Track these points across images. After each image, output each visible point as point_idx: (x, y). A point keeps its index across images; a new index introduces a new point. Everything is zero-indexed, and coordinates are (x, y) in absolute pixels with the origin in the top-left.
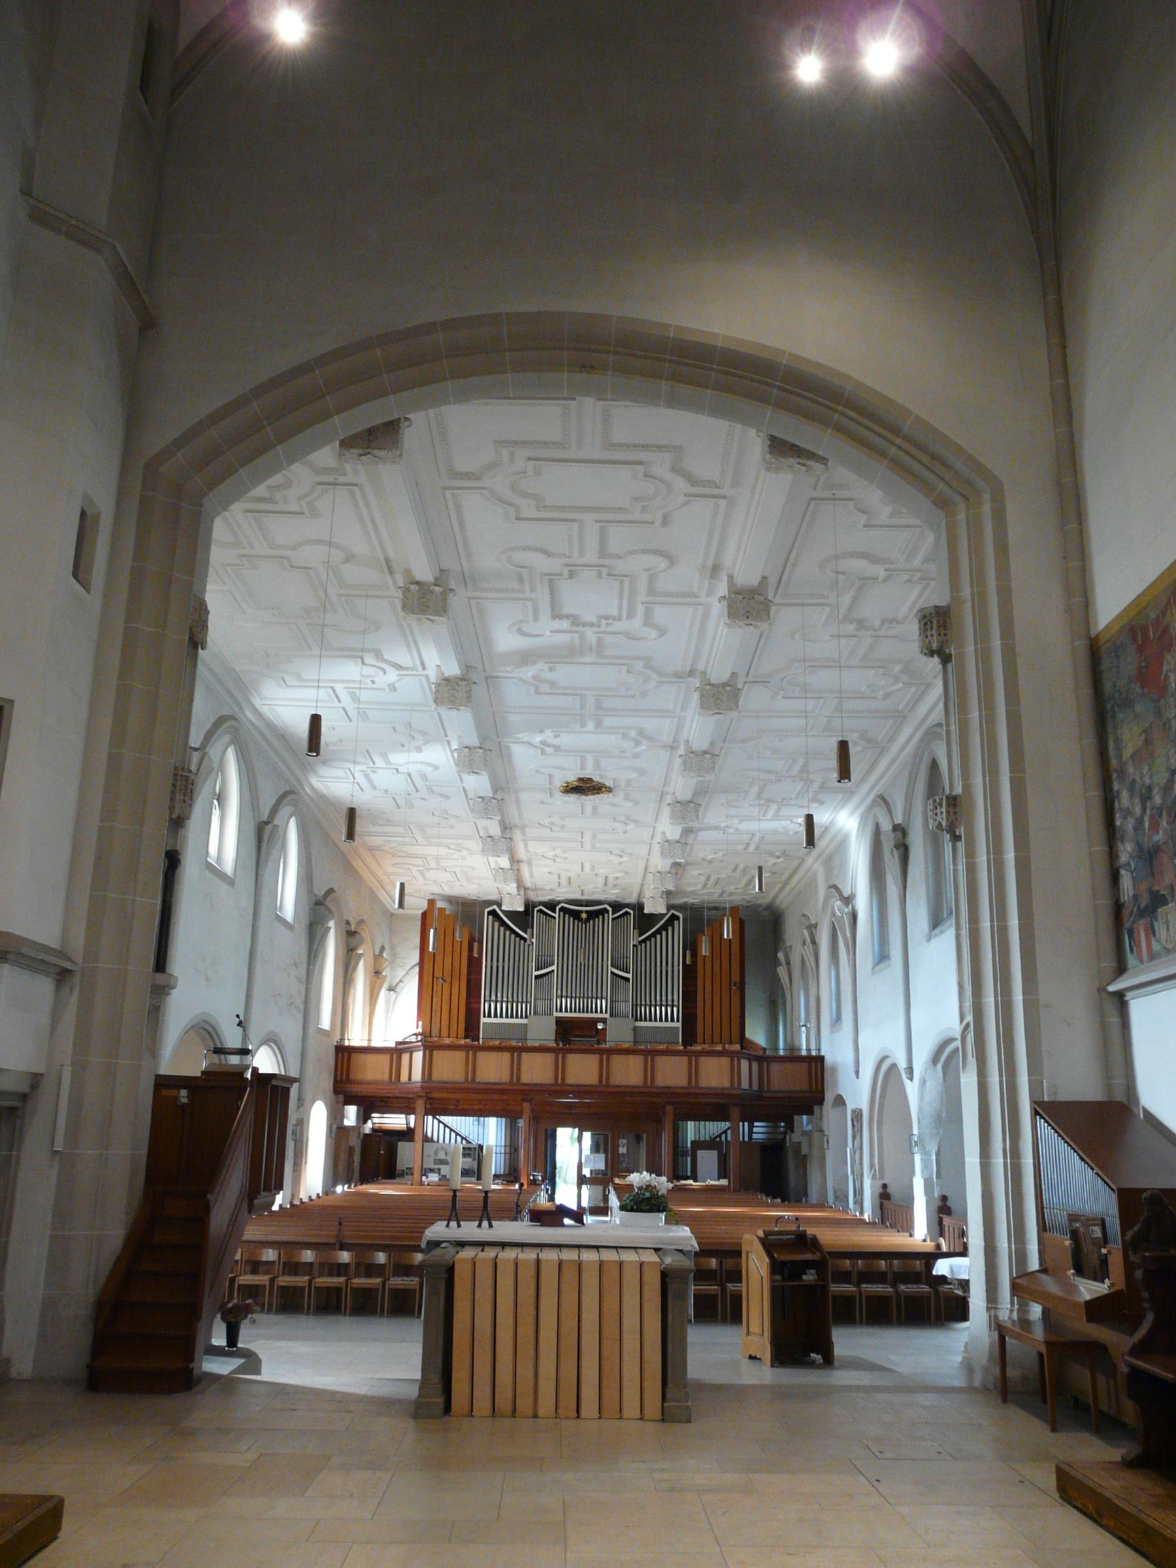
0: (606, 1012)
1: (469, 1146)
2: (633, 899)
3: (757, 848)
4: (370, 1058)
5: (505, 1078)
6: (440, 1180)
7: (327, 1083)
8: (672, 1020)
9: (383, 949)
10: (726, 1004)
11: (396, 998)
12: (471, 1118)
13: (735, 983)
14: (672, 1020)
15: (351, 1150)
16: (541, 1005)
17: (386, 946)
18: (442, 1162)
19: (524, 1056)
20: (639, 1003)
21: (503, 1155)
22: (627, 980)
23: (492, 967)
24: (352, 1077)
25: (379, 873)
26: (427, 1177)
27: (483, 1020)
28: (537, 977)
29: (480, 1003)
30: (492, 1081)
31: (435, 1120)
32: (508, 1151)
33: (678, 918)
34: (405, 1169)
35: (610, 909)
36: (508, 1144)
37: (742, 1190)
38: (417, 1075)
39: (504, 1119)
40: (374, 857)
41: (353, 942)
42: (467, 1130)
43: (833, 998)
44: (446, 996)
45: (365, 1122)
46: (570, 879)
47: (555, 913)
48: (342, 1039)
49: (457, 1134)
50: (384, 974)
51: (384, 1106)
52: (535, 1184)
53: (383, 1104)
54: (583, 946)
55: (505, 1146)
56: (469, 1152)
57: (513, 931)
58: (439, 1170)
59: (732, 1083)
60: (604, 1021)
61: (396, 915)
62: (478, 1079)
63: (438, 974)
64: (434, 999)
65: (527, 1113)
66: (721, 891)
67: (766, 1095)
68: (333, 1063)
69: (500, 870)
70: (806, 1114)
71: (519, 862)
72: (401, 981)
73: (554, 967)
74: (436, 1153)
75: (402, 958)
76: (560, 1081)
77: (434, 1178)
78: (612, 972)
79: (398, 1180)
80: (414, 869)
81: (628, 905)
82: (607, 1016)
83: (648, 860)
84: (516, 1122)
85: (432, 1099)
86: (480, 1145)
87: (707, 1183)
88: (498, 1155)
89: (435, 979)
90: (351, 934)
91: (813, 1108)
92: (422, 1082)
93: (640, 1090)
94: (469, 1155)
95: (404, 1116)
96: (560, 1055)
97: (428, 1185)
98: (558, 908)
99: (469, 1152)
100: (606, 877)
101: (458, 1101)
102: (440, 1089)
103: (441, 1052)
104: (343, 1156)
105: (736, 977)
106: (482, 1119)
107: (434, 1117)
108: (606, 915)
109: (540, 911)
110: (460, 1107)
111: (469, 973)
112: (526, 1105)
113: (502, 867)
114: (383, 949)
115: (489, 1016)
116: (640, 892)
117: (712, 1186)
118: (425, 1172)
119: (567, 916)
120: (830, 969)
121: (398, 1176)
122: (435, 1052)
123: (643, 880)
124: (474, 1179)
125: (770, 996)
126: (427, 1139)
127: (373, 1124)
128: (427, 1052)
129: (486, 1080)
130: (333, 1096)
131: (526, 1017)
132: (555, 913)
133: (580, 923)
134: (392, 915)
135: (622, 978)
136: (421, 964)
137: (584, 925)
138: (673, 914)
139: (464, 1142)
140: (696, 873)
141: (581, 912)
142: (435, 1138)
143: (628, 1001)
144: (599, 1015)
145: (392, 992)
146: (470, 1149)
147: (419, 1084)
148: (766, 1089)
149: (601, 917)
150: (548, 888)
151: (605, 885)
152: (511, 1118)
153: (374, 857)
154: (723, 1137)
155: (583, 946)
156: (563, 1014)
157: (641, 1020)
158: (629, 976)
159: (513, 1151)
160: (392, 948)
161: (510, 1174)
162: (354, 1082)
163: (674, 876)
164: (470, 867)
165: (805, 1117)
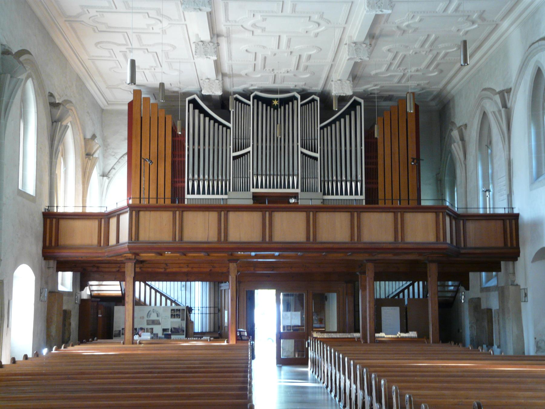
1: (178, 307)
2: (318, 88)
3: (456, 10)
4: (78, 224)
5: (213, 236)
6: (152, 338)
7: (36, 248)
8: (356, 193)
9: (94, 137)
10: (404, 180)
11: (109, 183)
12: (179, 283)
14: (356, 193)
15: (66, 314)
16: (239, 181)
17: (98, 135)
18: (154, 322)
21: (208, 315)
22: (316, 159)
23: (194, 150)
24: (62, 242)
25: (84, 57)
26: (140, 336)
27: (187, 196)
28: (235, 158)
29: (184, 182)
32: (212, 311)
34: (121, 329)
35: (299, 97)
36: (212, 305)
37: (441, 341)
38: (124, 237)
39: (208, 283)
40: (73, 29)
41: (58, 113)
42: (176, 295)
43: (534, 156)
45: (82, 289)
46: (265, 58)
47: (250, 100)
48: (51, 206)
49: (167, 298)
51: (96, 271)
52: (242, 340)
53: (95, 269)
55: (210, 307)
56: (178, 313)
57: (211, 118)
58: (152, 329)
59: (438, 237)
60: (295, 196)
61: (107, 110)
62: (186, 239)
63: (145, 155)
64: (143, 178)
65: (232, 277)
66: (402, 74)
67: (463, 251)
68: (41, 229)
70: (494, 271)
71: (218, 36)
72: (113, 168)
73: (250, 149)
74: (149, 315)
75: (113, 149)
77: (146, 336)
78: (302, 153)
79: (115, 340)
80: (117, 49)
82: (298, 191)
83: (344, 28)
84: (219, 287)
86: (187, 307)
87: (398, 335)
88: (204, 315)
89: (142, 160)
90: (54, 105)
91: (500, 263)
92: (129, 243)
94: (178, 316)
95: (118, 283)
96: (267, 213)
97: (140, 343)
98: (252, 96)
99: (178, 313)
100: (300, 56)
101: (166, 264)
103: (148, 213)
104: (57, 319)
105: (412, 153)
106: (188, 283)
107: (146, 284)
108: (295, 102)
109: (236, 99)
110: (168, 270)
111: (173, 155)
112: (233, 267)
113: (202, 39)
114: (94, 137)
115: (193, 193)
117: (402, 338)
118: (135, 331)
120: (529, 128)
121: (116, 336)
122: (142, 213)
124: (183, 337)
125: (438, 174)
126: (137, 303)
127: (91, 291)
128: (134, 213)
129: (194, 240)
130: (44, 262)
131: (226, 194)
132: (250, 100)
134: (103, 110)
135: (311, 157)
137: (276, 111)
138: (355, 101)
139: (173, 304)
140: (385, 48)
141: (274, 99)
142: (148, 302)
143: (317, 178)
144: (291, 191)
145: (105, 178)
146: (179, 310)
147: (127, 245)
148: (462, 245)
150: (243, 73)
151: (297, 69)
153: (73, 29)
154: (401, 295)
157: (328, 194)
158: (317, 155)
159: (217, 312)
160: (104, 139)
161: (214, 331)
162: (65, 247)
163: (369, 46)
165: (484, 274)
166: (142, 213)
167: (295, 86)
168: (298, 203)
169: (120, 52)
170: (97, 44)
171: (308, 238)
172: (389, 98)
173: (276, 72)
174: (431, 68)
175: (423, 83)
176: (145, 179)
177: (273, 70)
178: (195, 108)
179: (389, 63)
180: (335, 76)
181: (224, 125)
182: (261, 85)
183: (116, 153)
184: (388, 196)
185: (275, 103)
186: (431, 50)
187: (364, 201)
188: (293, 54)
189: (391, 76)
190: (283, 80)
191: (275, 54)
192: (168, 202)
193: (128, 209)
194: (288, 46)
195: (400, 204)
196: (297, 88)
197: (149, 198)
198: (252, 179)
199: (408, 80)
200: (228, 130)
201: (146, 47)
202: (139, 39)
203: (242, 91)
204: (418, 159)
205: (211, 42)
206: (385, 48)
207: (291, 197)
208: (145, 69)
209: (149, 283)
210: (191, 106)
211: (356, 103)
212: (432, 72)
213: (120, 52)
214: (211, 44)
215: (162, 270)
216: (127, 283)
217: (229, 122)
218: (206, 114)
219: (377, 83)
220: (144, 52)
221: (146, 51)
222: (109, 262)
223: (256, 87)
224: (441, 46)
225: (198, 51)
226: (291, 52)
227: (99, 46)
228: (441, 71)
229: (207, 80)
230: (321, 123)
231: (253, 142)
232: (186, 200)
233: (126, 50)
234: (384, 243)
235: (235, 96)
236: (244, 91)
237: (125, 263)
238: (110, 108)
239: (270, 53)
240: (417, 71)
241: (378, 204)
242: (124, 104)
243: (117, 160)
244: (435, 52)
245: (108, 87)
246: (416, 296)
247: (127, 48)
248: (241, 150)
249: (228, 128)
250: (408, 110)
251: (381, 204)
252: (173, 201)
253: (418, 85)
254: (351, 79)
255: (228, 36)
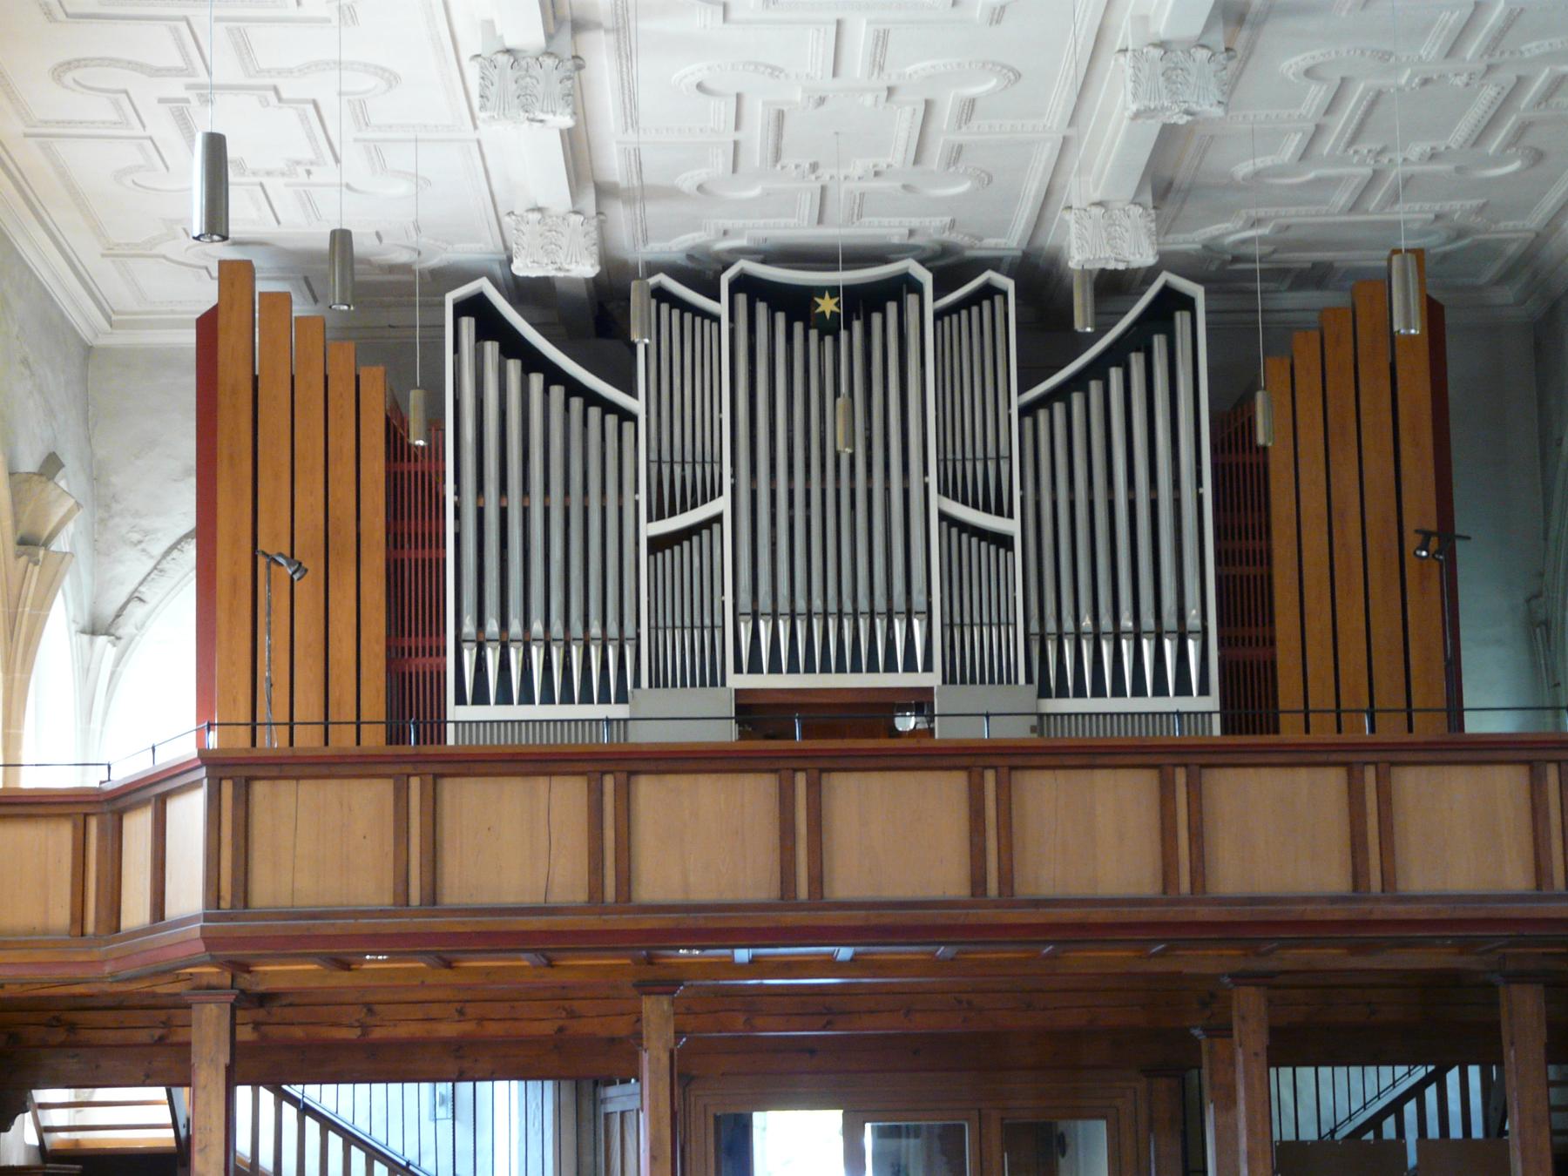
0: (928, 667)
2: (1010, 241)
8: (1183, 688)
9: (52, 465)
11: (118, 661)
12: (426, 1087)
13: (1427, 535)
16: (678, 645)
17: (68, 458)
19: (647, 789)
20: (1051, 626)
22: (1004, 541)
23: (480, 513)
27: (454, 712)
28: (656, 544)
30: (510, 898)
31: (286, 1107)
33: (1188, 303)
35: (926, 277)
39: (549, 1085)
44: (308, 632)
46: (780, 116)
47: (717, 298)
50: (61, 544)
51: (62, 1045)
53: (60, 1036)
54: (844, 389)
57: (554, 375)
60: (920, 701)
61: (107, 351)
62: (455, 892)
63: (273, 540)
64: (263, 638)
65: (654, 1058)
66: (1367, 171)
69: (504, 60)
71: (579, 26)
72: (135, 597)
73: (722, 505)
75: (137, 514)
76: (803, 892)
78: (943, 516)
81: (995, 264)
82: (933, 680)
84: (597, 1102)
85: (264, 999)
89: (262, 561)
92: (207, 918)
93: (1145, 914)
95: (159, 1093)
96: (801, 779)
100: (928, 105)
101: (369, 1008)
102: (290, 945)
103: (286, 787)
105: (1420, 510)
106: (465, 1088)
107: (282, 1097)
108: (912, 300)
109: (660, 294)
110: (377, 1034)
111: (394, 538)
112: (656, 1012)
113: (509, 44)
114: (52, 465)
115: (481, 698)
116: (1048, 193)
119: (762, 309)
122: (260, 789)
123: (1072, 122)
127: (43, 1131)
128: (227, 788)
129: (486, 899)
131: (622, 698)
132: (717, 298)
133: (814, 334)
134: (88, 351)
136: (206, 533)
137: (828, 340)
140: (1291, 65)
141: (820, 291)
144: (900, 680)
145: (102, 640)
149: (892, 308)
150: (687, 181)
152: (578, 1082)
155: (844, 389)
156: (764, 681)
157: (1062, 692)
158: (1011, 526)
160: (96, 476)
163: (1222, 57)
164: (379, 71)
166: (449, 787)
167: (912, 233)
168: (931, 731)
169: (161, 101)
170: (60, 71)
171: (978, 881)
172: (1316, 276)
173: (825, 173)
174: (1493, 145)
175: (1459, 207)
176: (272, 643)
177: (814, 167)
178: (482, 335)
179: (1311, 127)
180: (1081, 188)
181: (609, 407)
182: (762, 234)
183: (146, 533)
184: (1321, 696)
185: (827, 305)
186: (1490, 68)
187: (1216, 719)
188: (897, 98)
189: (1319, 182)
190: (860, 205)
191: (822, 101)
192: (374, 738)
193: (203, 772)
194: (878, 64)
195: (1372, 729)
196: (915, 241)
197: (358, 724)
198: (733, 634)
199: (1394, 198)
200: (628, 427)
201: (269, 81)
202: (243, 48)
203: (681, 259)
204: (1444, 536)
205: (548, 53)
206: (1291, 65)
207: (903, 709)
208: (269, 173)
209: (295, 1090)
210: (468, 324)
211: (1171, 301)
212: (1498, 160)
213: (161, 101)
214: (549, 62)
215: (353, 1034)
216: (199, 1092)
217: (631, 391)
218: (533, 361)
219: (1262, 212)
220: (265, 103)
221: (271, 95)
222: (119, 1004)
223: (742, 242)
224: (1532, 48)
225: (492, 91)
226: (891, 91)
227: (68, 78)
228: (1538, 157)
229: (536, 216)
230: (1021, 391)
231: (734, 475)
232: (450, 728)
233: (182, 93)
234: (1307, 900)
235: (653, 281)
236: (690, 257)
237: (188, 1007)
238: (119, 339)
239: (798, 96)
240: (1434, 156)
241: (1276, 731)
242: (178, 325)
243: (151, 564)
244: (1507, 76)
245: (112, 253)
246: (1456, 1132)
247: (189, 87)
248: (672, 513)
249: (626, 416)
250: (1398, 326)
251: (1291, 730)
252: (396, 735)
253: (1438, 217)
254: (1148, 198)
255: (621, 29)
